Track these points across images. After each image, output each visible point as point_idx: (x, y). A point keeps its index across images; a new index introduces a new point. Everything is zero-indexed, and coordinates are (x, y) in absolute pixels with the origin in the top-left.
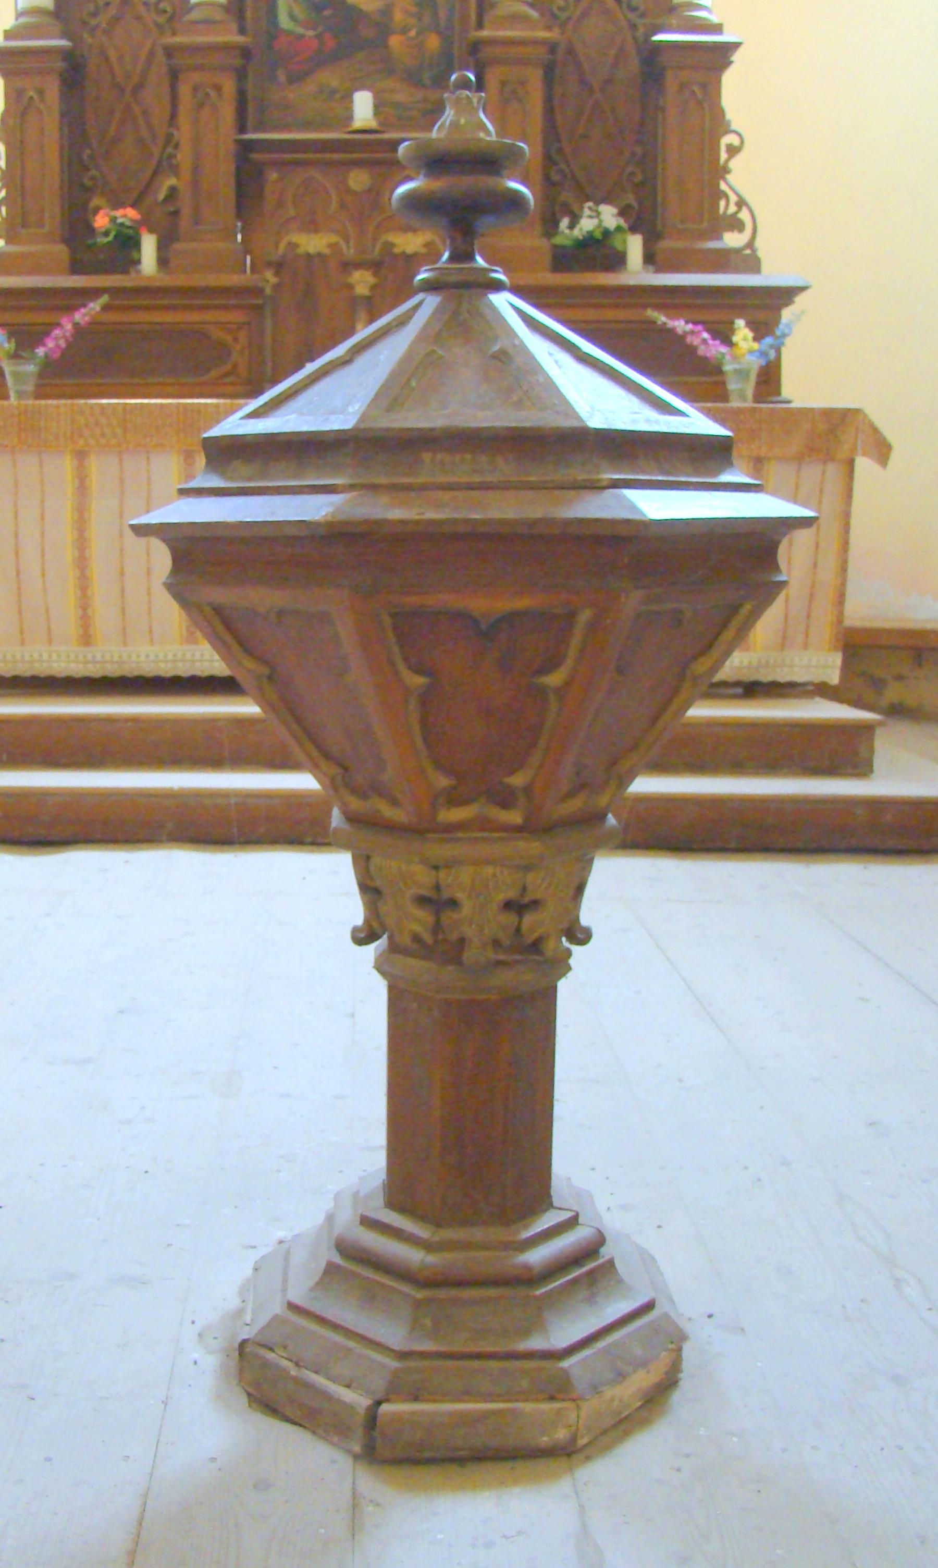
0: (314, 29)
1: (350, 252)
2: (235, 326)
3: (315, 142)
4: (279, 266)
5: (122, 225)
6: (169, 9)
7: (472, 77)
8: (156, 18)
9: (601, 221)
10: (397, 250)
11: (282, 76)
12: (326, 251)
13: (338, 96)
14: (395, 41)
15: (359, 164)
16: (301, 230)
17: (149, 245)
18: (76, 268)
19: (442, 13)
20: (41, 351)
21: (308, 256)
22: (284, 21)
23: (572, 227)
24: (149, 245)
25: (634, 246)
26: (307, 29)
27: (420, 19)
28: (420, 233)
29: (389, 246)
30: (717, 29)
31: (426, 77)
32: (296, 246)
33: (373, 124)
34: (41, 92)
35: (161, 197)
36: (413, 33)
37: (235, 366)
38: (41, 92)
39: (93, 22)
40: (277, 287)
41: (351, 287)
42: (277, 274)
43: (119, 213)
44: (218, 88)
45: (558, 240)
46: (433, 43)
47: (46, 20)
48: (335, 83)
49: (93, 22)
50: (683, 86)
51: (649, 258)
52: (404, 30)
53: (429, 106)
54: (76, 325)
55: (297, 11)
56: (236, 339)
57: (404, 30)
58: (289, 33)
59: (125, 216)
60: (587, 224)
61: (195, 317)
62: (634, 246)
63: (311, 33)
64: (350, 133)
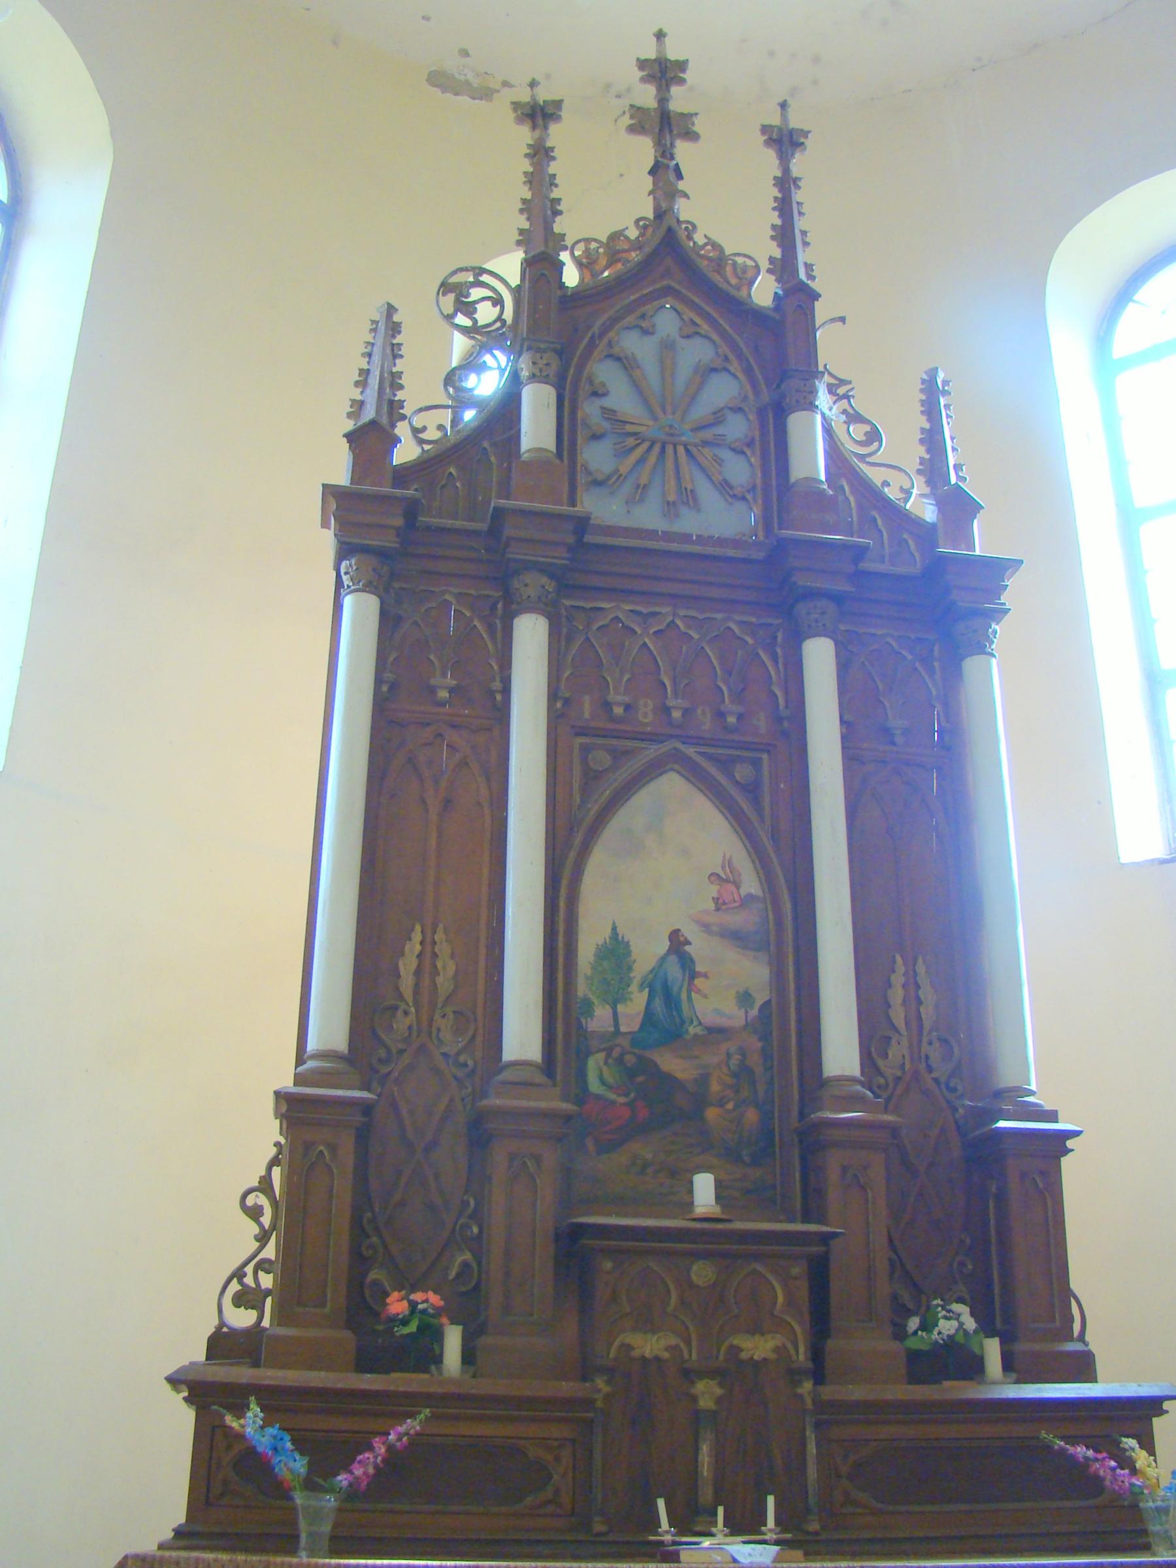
0: (626, 1095)
1: (693, 1356)
2: (555, 1443)
3: (625, 1228)
4: (609, 1372)
5: (424, 1311)
6: (470, 1063)
7: (968, 1241)
8: (454, 1070)
9: (961, 1324)
10: (744, 1356)
11: (590, 1143)
12: (666, 1355)
13: (649, 1171)
14: (711, 1114)
15: (707, 1255)
16: (634, 1329)
17: (453, 1341)
18: (364, 1363)
19: (761, 1089)
20: (342, 1479)
21: (644, 1360)
22: (594, 1086)
23: (925, 1326)
24: (453, 1341)
25: (992, 1350)
26: (619, 1095)
27: (737, 1091)
28: (769, 1336)
29: (735, 1350)
30: (1052, 1116)
31: (745, 1154)
32: (629, 1347)
33: (715, 1210)
34: (333, 1148)
35: (452, 1274)
36: (730, 1106)
37: (557, 1492)
38: (333, 1148)
39: (384, 1070)
40: (607, 1397)
41: (694, 1399)
42: (608, 1382)
43: (417, 1296)
44: (538, 1159)
45: (912, 1343)
46: (752, 1116)
47: (342, 1066)
48: (649, 1156)
49: (384, 1070)
50: (1023, 1176)
51: (1008, 1364)
52: (721, 1104)
54: (390, 1448)
56: (557, 1459)
57: (721, 1104)
58: (598, 1097)
59: (426, 1301)
60: (946, 1327)
61: (508, 1430)
62: (992, 1350)
63: (622, 1100)
64: (694, 1220)
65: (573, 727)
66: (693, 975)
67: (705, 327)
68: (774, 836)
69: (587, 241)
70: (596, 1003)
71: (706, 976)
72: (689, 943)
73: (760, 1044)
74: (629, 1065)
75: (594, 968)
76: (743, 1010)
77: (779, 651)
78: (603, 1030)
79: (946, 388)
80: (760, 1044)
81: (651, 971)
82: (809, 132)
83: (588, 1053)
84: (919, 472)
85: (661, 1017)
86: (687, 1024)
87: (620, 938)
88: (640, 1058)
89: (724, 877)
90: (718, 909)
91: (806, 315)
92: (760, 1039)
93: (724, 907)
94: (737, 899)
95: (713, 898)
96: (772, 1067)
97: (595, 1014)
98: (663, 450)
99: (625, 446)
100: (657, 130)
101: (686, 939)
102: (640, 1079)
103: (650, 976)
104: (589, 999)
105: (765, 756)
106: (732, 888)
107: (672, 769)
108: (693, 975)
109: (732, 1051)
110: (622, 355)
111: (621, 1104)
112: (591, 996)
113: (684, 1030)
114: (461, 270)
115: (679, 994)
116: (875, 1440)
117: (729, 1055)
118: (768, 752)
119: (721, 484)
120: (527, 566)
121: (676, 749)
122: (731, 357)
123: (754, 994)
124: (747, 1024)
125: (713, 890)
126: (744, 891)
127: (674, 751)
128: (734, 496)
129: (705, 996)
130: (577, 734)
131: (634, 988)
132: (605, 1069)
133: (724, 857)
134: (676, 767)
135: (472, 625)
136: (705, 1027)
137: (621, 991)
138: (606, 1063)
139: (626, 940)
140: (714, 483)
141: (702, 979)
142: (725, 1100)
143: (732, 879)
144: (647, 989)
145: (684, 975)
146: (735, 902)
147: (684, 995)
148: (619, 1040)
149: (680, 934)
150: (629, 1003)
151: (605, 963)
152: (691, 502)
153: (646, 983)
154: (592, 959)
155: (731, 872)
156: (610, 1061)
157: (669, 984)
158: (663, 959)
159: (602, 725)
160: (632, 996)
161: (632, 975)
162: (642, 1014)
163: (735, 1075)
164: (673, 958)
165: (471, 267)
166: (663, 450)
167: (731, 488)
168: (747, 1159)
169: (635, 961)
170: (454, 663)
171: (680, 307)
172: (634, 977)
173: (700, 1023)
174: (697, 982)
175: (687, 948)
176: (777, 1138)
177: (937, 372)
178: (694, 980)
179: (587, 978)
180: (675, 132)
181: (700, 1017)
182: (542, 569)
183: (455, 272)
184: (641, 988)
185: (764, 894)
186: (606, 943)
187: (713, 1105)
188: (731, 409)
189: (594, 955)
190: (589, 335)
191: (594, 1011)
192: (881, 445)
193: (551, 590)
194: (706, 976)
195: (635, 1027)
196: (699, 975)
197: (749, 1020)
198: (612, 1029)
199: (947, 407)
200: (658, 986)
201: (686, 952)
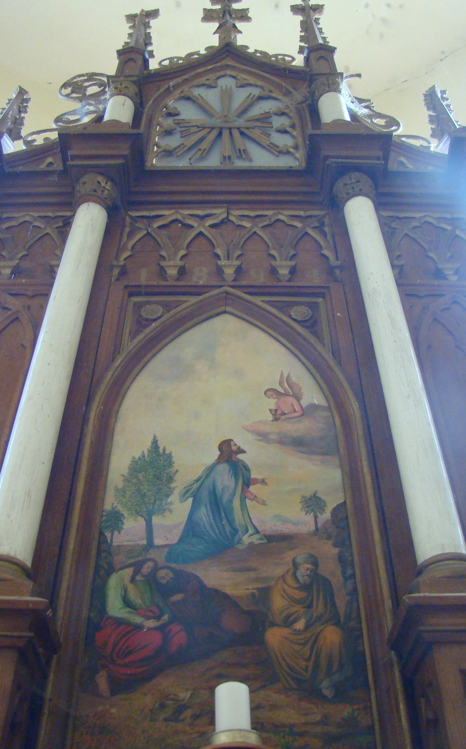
0: (158, 618)
13: (188, 713)
36: (300, 625)
48: (184, 695)
53: (333, 730)
55: (133, 595)
58: (119, 622)
63: (151, 623)
65: (126, 287)
66: (248, 483)
67: (252, 80)
68: (335, 354)
69: (169, 59)
70: (126, 515)
71: (263, 482)
72: (243, 452)
73: (335, 551)
74: (164, 582)
75: (126, 480)
76: (312, 514)
77: (327, 229)
78: (133, 543)
79: (444, 96)
80: (335, 551)
81: (197, 481)
82: (323, 5)
83: (111, 570)
84: (433, 136)
85: (208, 527)
86: (240, 532)
87: (161, 450)
88: (178, 574)
89: (282, 391)
90: (276, 419)
91: (327, 60)
92: (335, 545)
93: (283, 417)
94: (297, 408)
95: (270, 410)
96: (353, 575)
97: (124, 527)
98: (220, 134)
99: (190, 131)
100: (221, 16)
101: (239, 448)
102: (178, 597)
103: (195, 486)
104: (117, 512)
105: (320, 300)
106: (291, 400)
107: (225, 312)
108: (248, 483)
109: (299, 560)
110: (190, 96)
111: (149, 629)
112: (120, 508)
113: (236, 538)
114: (80, 76)
115: (231, 501)
116: (285, 661)
117: (295, 565)
118: (323, 296)
119: (261, 134)
120: (86, 169)
121: (227, 293)
122: (272, 88)
123: (323, 497)
124: (317, 529)
125: (272, 403)
126: (305, 402)
127: (225, 294)
128: (280, 152)
129: (264, 503)
130: (131, 295)
131: (174, 498)
132: (131, 587)
133: (282, 375)
134: (228, 309)
135: (46, 232)
136: (265, 536)
137: (158, 502)
138: (133, 580)
139: (167, 452)
140: (263, 147)
141: (258, 486)
142: (291, 619)
143: (291, 393)
144: (191, 500)
145: (236, 484)
146: (295, 411)
147: (236, 503)
148: (152, 554)
149: (232, 443)
150: (167, 514)
151: (140, 476)
152: (244, 156)
153: (190, 492)
154: (125, 471)
155: (290, 387)
156: (138, 578)
157: (219, 496)
158: (210, 470)
159: (155, 283)
160: (172, 507)
161: (172, 485)
162: (182, 527)
163: (305, 587)
164: (224, 468)
165: (86, 74)
166: (220, 134)
167: (278, 147)
168: (328, 693)
169: (177, 471)
170: (23, 256)
171: (233, 73)
172: (174, 488)
173: (257, 532)
174: (252, 489)
175: (240, 456)
176: (369, 662)
177: (435, 88)
178: (248, 488)
179: (117, 489)
180: (233, 16)
181: (256, 524)
182: (98, 170)
183: (75, 78)
184: (184, 496)
185: (328, 402)
186: (144, 456)
187: (277, 625)
188: (276, 114)
189: (129, 467)
190: (166, 86)
191: (123, 523)
192: (398, 129)
193: (107, 187)
194: (263, 482)
195: (174, 538)
196: (256, 481)
197: (319, 525)
198: (145, 542)
199: (448, 106)
200: (205, 495)
201: (239, 460)
